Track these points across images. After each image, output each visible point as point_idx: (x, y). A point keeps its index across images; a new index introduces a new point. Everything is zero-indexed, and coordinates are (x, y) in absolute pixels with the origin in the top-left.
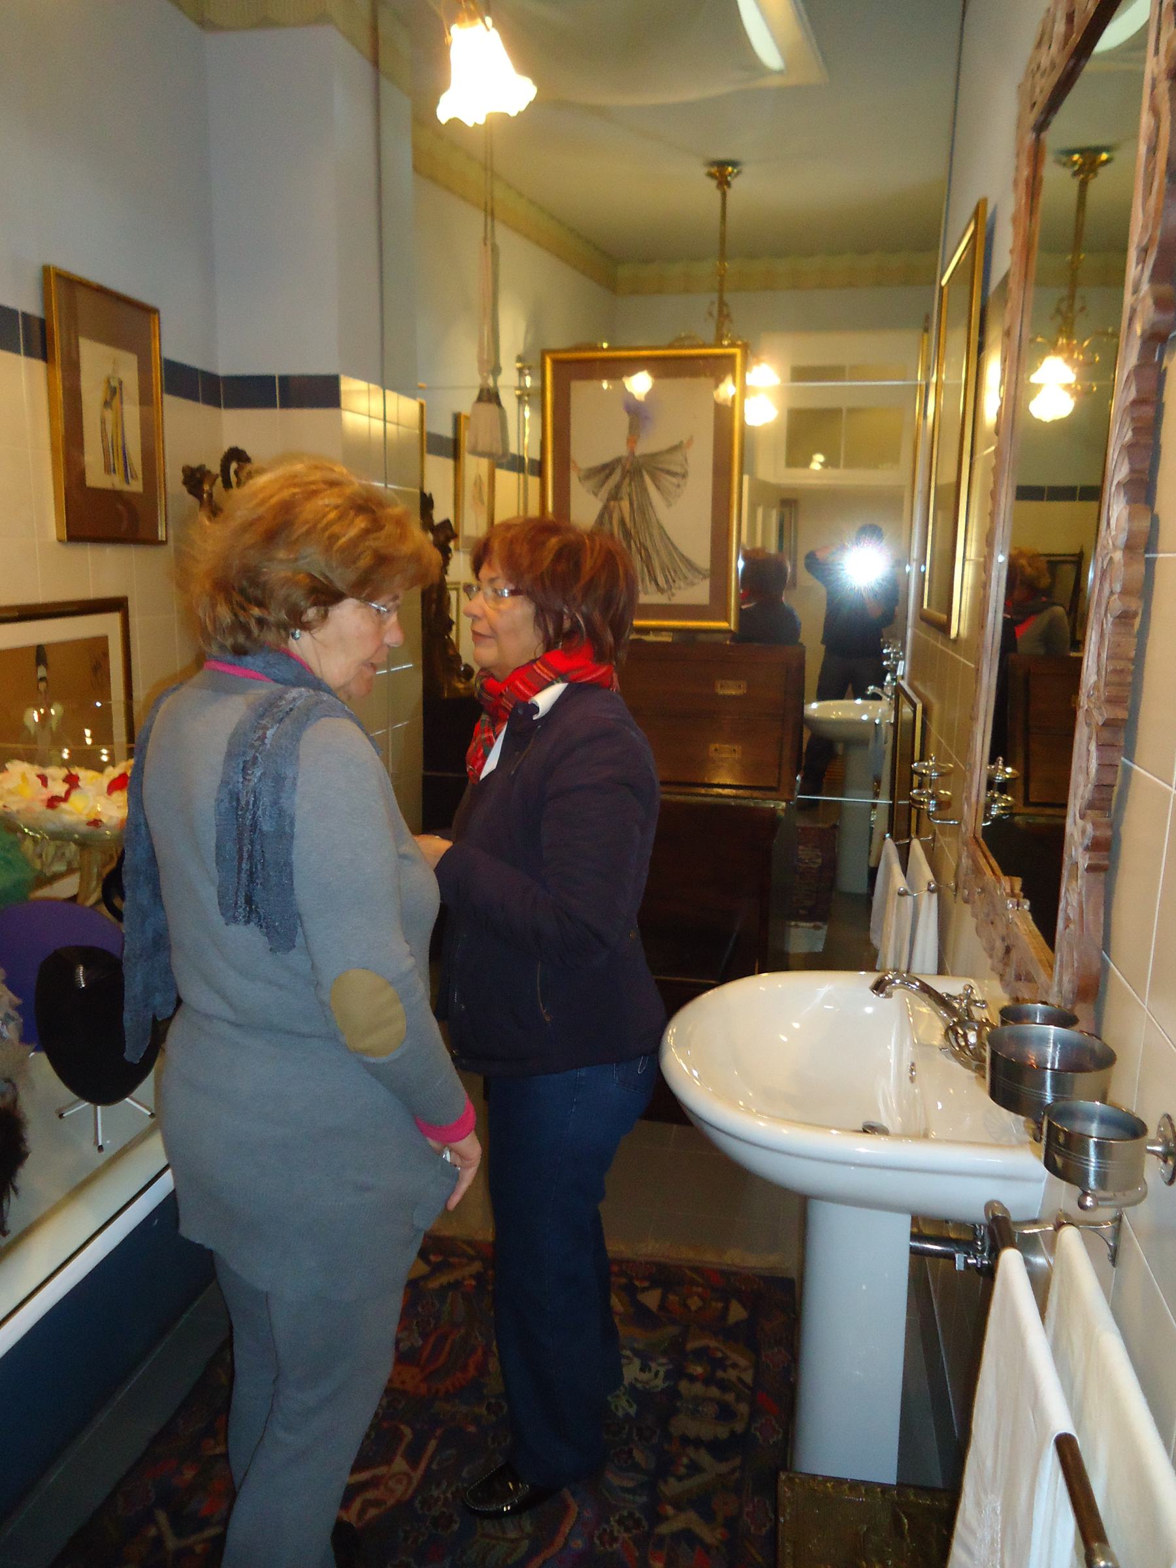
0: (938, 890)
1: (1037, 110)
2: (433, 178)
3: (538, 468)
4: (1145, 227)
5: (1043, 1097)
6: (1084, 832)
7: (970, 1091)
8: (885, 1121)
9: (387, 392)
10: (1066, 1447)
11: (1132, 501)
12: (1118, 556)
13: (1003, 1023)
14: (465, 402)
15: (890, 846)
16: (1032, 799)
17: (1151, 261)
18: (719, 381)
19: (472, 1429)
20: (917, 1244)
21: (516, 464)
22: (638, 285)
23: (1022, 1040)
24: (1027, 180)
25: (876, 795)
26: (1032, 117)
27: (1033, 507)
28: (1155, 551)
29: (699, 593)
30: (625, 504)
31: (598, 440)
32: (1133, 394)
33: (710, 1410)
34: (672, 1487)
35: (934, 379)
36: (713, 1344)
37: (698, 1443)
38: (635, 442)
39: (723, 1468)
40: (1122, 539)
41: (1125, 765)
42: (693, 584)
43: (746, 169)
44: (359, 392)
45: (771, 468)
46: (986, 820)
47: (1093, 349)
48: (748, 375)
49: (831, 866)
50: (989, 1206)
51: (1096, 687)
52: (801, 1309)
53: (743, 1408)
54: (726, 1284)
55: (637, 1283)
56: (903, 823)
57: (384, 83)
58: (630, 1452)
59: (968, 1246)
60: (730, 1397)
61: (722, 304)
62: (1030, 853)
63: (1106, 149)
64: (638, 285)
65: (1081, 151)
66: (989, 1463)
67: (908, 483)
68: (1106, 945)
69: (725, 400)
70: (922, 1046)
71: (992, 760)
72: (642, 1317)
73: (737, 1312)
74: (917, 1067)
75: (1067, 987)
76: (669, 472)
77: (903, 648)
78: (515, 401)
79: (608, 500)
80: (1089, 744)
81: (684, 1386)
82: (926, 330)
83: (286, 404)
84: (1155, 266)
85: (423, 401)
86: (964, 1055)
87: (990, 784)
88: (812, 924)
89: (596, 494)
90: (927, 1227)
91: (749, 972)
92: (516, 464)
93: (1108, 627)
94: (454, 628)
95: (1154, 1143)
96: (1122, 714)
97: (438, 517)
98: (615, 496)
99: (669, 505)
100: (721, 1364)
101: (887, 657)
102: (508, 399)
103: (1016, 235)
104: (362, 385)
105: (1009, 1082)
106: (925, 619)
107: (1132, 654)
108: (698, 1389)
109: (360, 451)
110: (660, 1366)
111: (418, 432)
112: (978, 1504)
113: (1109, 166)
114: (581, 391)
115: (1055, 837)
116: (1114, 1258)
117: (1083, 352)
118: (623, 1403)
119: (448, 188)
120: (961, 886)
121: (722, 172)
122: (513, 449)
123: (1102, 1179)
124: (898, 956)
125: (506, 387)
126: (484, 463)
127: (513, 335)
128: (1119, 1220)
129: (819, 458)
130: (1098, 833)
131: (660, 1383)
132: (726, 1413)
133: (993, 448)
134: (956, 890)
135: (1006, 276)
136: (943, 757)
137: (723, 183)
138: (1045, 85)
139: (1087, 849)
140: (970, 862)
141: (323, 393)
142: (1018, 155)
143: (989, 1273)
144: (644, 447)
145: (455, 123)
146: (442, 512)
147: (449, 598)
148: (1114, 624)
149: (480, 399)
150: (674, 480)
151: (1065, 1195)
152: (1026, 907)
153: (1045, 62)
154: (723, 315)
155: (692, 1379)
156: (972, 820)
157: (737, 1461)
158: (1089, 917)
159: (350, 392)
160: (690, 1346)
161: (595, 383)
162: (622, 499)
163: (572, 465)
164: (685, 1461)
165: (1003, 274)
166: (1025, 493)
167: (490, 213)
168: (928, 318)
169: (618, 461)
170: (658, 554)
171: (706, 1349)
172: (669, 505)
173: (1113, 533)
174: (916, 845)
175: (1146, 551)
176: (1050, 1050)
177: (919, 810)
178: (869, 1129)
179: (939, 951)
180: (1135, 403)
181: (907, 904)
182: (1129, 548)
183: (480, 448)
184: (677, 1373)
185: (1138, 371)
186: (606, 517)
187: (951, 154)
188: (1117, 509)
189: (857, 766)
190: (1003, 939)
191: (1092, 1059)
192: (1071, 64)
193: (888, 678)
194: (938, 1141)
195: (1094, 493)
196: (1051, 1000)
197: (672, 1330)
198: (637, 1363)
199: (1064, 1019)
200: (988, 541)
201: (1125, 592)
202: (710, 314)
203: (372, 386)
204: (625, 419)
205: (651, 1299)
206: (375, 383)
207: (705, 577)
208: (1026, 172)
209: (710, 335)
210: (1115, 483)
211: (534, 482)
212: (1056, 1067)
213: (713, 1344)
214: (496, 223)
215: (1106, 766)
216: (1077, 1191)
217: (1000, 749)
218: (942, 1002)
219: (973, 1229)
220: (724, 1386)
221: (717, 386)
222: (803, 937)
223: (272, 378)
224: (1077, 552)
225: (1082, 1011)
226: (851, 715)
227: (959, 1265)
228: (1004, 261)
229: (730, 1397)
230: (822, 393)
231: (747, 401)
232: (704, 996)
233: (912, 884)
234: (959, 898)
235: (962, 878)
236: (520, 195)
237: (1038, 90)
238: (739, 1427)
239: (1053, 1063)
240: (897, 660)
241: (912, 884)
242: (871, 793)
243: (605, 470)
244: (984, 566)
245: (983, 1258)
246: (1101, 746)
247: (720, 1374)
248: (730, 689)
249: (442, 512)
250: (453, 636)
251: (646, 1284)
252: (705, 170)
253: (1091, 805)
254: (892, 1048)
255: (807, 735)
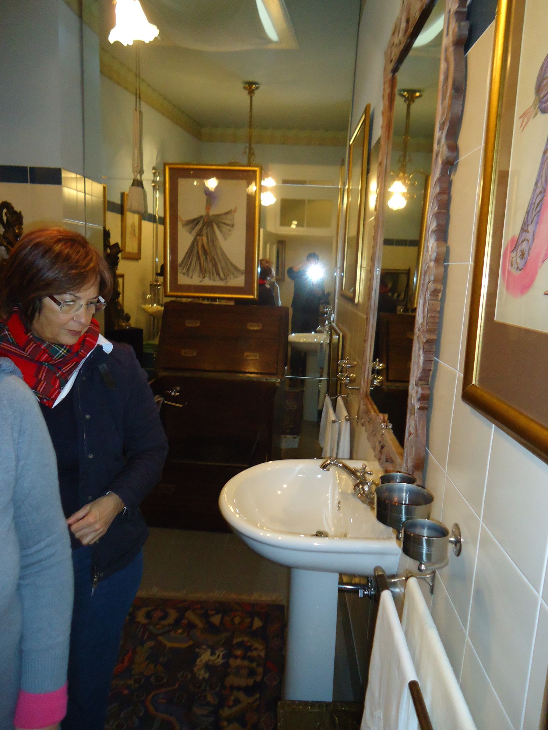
0: (349, 419)
1: (393, 63)
2: (110, 78)
3: (162, 221)
4: (443, 114)
5: (401, 518)
6: (417, 392)
7: (370, 515)
8: (325, 528)
9: (86, 179)
10: (414, 687)
11: (438, 240)
12: (432, 264)
13: (382, 483)
14: (126, 186)
15: (328, 400)
16: (390, 379)
17: (446, 129)
18: (249, 184)
19: (126, 692)
20: (341, 586)
21: (152, 218)
22: (211, 140)
23: (391, 490)
24: (389, 94)
25: (321, 376)
26: (391, 66)
27: (389, 248)
28: (448, 262)
29: (239, 281)
30: (204, 238)
31: (191, 208)
32: (438, 190)
33: (244, 672)
34: (226, 712)
35: (347, 187)
36: (246, 639)
37: (239, 688)
38: (209, 208)
39: (251, 700)
40: (434, 256)
41: (435, 360)
42: (236, 277)
43: (262, 87)
44: (72, 178)
45: (273, 226)
46: (371, 387)
47: (414, 179)
48: (262, 181)
49: (300, 411)
50: (376, 569)
51: (422, 325)
52: (288, 620)
53: (260, 670)
54: (251, 610)
55: (209, 612)
56: (334, 390)
57: (85, 27)
58: (205, 696)
59: (365, 587)
60: (254, 665)
61: (250, 149)
62: (392, 402)
63: (419, 91)
64: (211, 140)
65: (408, 91)
66: (377, 694)
67: (335, 235)
68: (427, 444)
69: (252, 193)
70: (343, 493)
71: (374, 360)
72: (211, 629)
73: (258, 623)
74: (341, 502)
75: (410, 464)
76: (225, 224)
77: (334, 309)
78: (152, 189)
79: (196, 236)
80: (419, 351)
81: (232, 661)
82: (343, 164)
83: (33, 181)
84: (448, 131)
85: (105, 185)
86: (366, 499)
87: (374, 371)
88: (292, 436)
89: (190, 233)
90: (344, 576)
91: (264, 461)
92: (152, 218)
93: (428, 297)
94: (121, 295)
95: (451, 537)
96: (434, 337)
97: (112, 241)
98: (199, 234)
99: (226, 239)
100: (250, 648)
101: (326, 313)
102: (148, 186)
103: (383, 121)
104: (73, 175)
105: (386, 512)
106: (343, 296)
107: (439, 309)
108: (239, 662)
109: (72, 209)
110: (220, 652)
111: (102, 200)
112: (372, 716)
113: (420, 99)
114: (183, 183)
115: (404, 395)
116: (432, 591)
117: (410, 180)
118: (202, 672)
119: (118, 83)
120: (360, 418)
121: (251, 87)
122: (150, 211)
123: (429, 556)
124: (332, 451)
125: (147, 180)
126: (136, 216)
127: (150, 157)
128: (434, 573)
129: (295, 222)
130: (424, 392)
131: (220, 661)
132: (252, 673)
133: (373, 218)
134: (358, 419)
135: (379, 141)
136: (352, 359)
137: (251, 92)
138: (396, 52)
139: (419, 400)
140: (365, 407)
141: (53, 177)
142: (384, 83)
143: (376, 599)
144: (213, 212)
145: (117, 43)
146: (115, 239)
147: (118, 282)
148: (430, 295)
149: (133, 185)
150: (228, 228)
151: (410, 563)
152: (390, 427)
153: (396, 41)
154: (251, 153)
155: (236, 657)
156: (365, 387)
157: (258, 695)
158: (420, 431)
159: (67, 178)
160: (235, 641)
161: (190, 180)
162: (203, 235)
163: (179, 218)
164: (233, 698)
165: (377, 138)
166: (388, 242)
167: (138, 96)
168: (343, 160)
169: (201, 217)
170: (221, 263)
171: (242, 642)
172: (226, 239)
173: (430, 253)
174: (340, 400)
175: (444, 262)
176: (404, 494)
177: (341, 383)
178: (319, 534)
179: (351, 448)
180: (439, 194)
181: (336, 426)
182: (437, 260)
183: (133, 208)
184: (228, 656)
185: (440, 180)
186: (195, 243)
187: (353, 92)
188: (431, 244)
189: (311, 364)
190: (380, 442)
191: (423, 499)
192: (409, 40)
193: (327, 322)
194: (351, 538)
195: (416, 243)
196: (402, 470)
197: (225, 635)
198: (209, 652)
199: (410, 481)
200: (372, 259)
201: (435, 281)
202: (245, 152)
203: (78, 176)
204: (205, 198)
205: (216, 619)
206: (80, 174)
207: (242, 274)
208: (388, 91)
209: (245, 160)
210: (431, 230)
211: (161, 228)
212: (407, 502)
213: (246, 639)
214: (141, 102)
215: (427, 361)
216: (418, 563)
217: (377, 355)
218: (352, 472)
219: (367, 578)
220: (251, 660)
221: (248, 186)
222: (288, 442)
223: (27, 167)
224: (408, 269)
225: (417, 475)
226: (310, 340)
227: (361, 595)
228: (378, 132)
229: (254, 665)
230: (296, 193)
231: (262, 194)
232: (243, 472)
233: (338, 417)
234: (359, 424)
235: (360, 415)
236: (154, 90)
237: (393, 54)
238: (259, 678)
239: (406, 501)
240: (331, 314)
241: (338, 417)
242: (319, 375)
243: (194, 222)
244: (370, 271)
245: (371, 591)
246: (425, 352)
247: (249, 654)
248: (254, 327)
249: (115, 239)
250: (120, 300)
251: (214, 612)
252: (243, 85)
253: (420, 379)
254: (329, 495)
255: (289, 350)
